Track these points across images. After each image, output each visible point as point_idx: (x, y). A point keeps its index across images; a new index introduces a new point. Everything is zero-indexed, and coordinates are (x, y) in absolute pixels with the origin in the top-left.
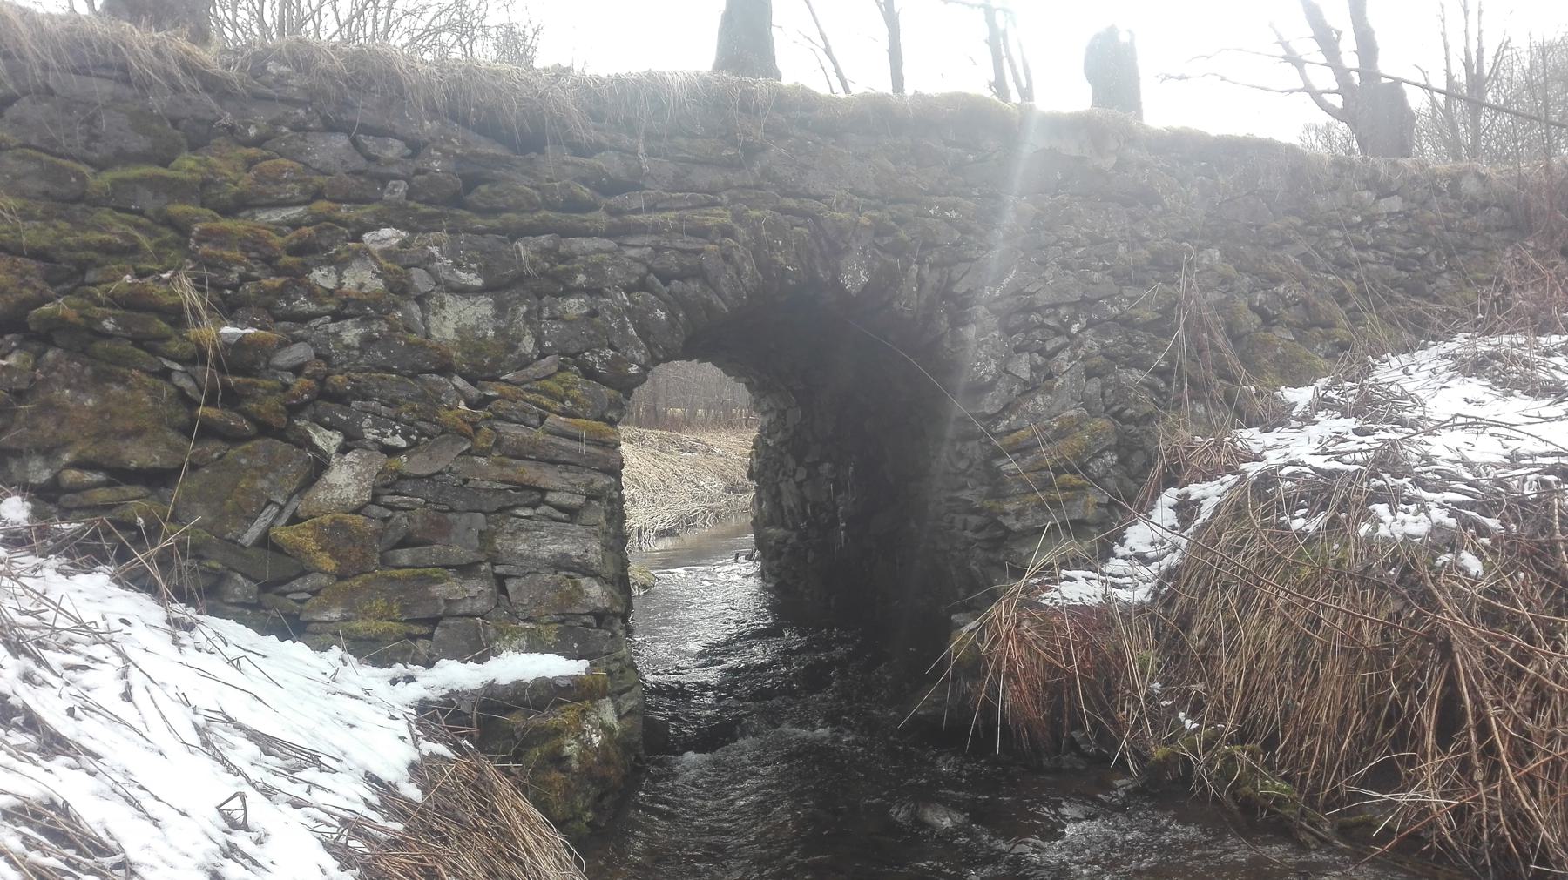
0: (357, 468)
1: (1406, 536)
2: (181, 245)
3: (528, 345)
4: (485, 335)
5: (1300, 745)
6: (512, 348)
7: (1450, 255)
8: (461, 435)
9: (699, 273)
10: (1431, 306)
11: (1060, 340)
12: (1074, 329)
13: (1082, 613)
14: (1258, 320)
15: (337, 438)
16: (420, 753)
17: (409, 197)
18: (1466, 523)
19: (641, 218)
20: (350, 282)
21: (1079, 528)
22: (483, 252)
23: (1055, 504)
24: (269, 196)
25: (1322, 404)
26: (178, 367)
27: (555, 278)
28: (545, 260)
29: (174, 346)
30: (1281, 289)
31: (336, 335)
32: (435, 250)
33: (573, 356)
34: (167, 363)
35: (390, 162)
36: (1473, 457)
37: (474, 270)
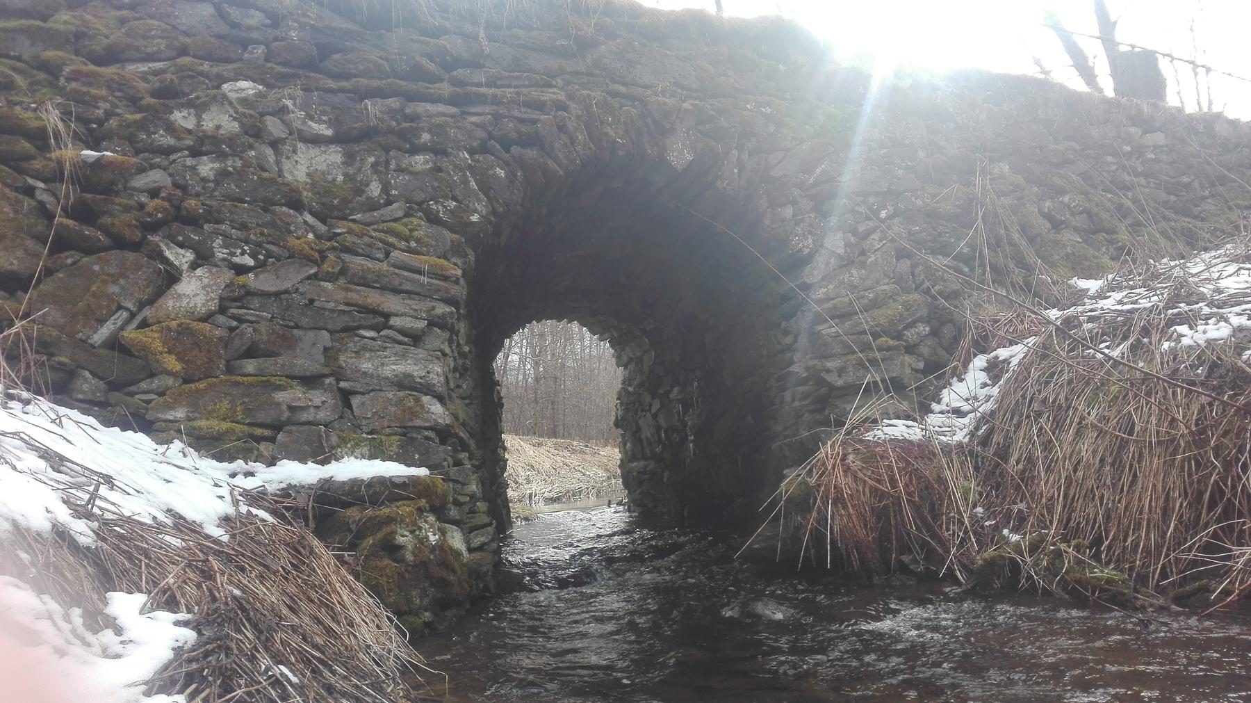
0: (206, 281)
1: (1209, 342)
2: (53, 85)
3: (375, 189)
4: (334, 180)
5: (1125, 540)
6: (359, 191)
7: (1213, 185)
8: (311, 260)
9: (533, 141)
10: (1199, 224)
11: (871, 224)
12: (883, 214)
13: (904, 446)
14: (1048, 225)
15: (189, 256)
16: (237, 511)
17: (267, 60)
19: (483, 90)
20: (208, 124)
21: (897, 386)
22: (334, 107)
23: (874, 362)
24: (137, 49)
26: (41, 185)
27: (402, 135)
28: (392, 118)
29: (37, 164)
30: (1066, 199)
31: (193, 168)
32: (289, 103)
33: (420, 204)
34: (30, 181)
35: (250, 28)
37: (325, 122)
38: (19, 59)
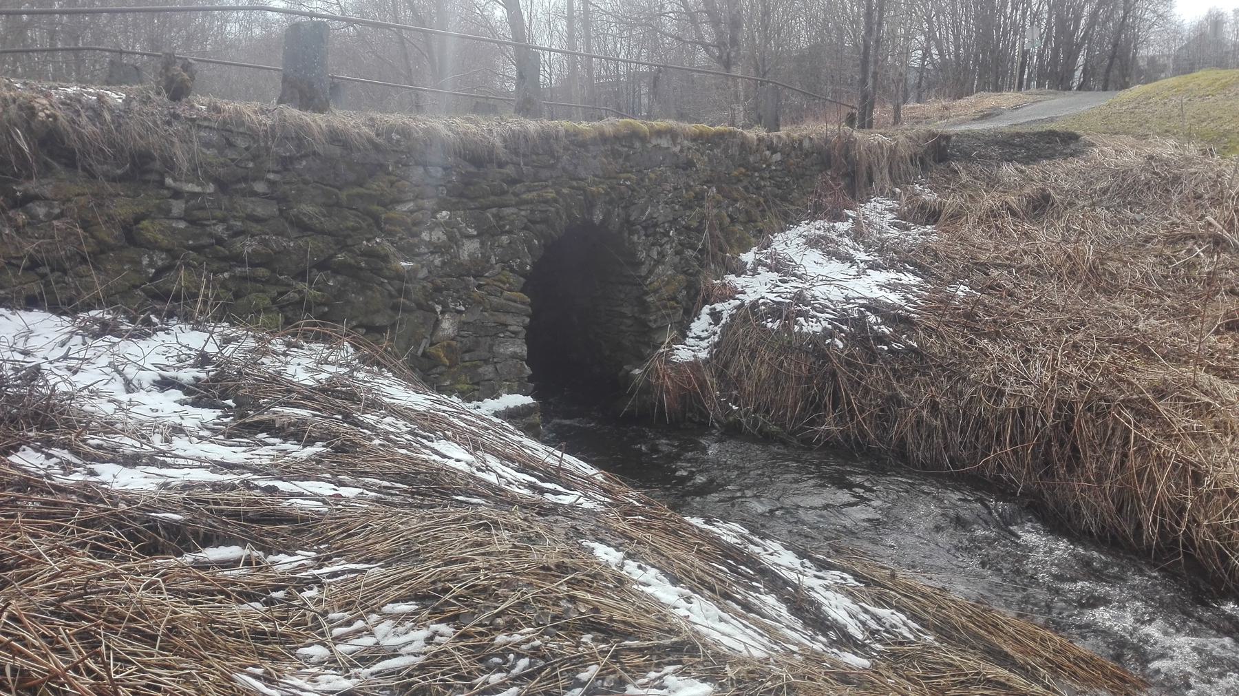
6: (488, 262)
9: (545, 221)
18: (835, 327)
23: (669, 315)
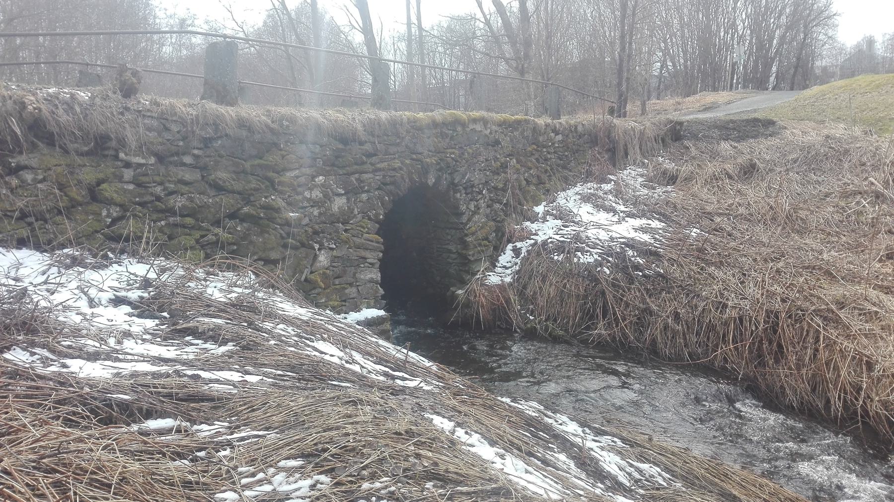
6: (352, 213)
18: (603, 259)
23: (483, 251)
25: (547, 213)
36: (600, 237)
38: (258, 175)
